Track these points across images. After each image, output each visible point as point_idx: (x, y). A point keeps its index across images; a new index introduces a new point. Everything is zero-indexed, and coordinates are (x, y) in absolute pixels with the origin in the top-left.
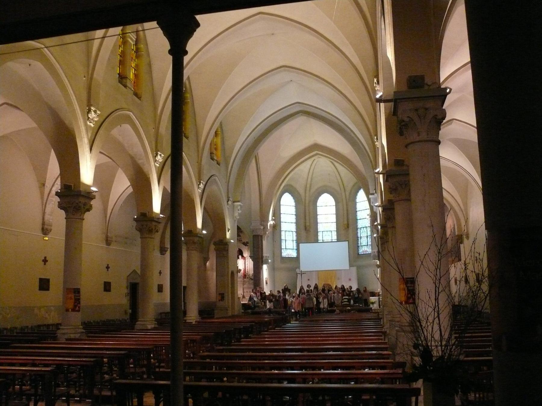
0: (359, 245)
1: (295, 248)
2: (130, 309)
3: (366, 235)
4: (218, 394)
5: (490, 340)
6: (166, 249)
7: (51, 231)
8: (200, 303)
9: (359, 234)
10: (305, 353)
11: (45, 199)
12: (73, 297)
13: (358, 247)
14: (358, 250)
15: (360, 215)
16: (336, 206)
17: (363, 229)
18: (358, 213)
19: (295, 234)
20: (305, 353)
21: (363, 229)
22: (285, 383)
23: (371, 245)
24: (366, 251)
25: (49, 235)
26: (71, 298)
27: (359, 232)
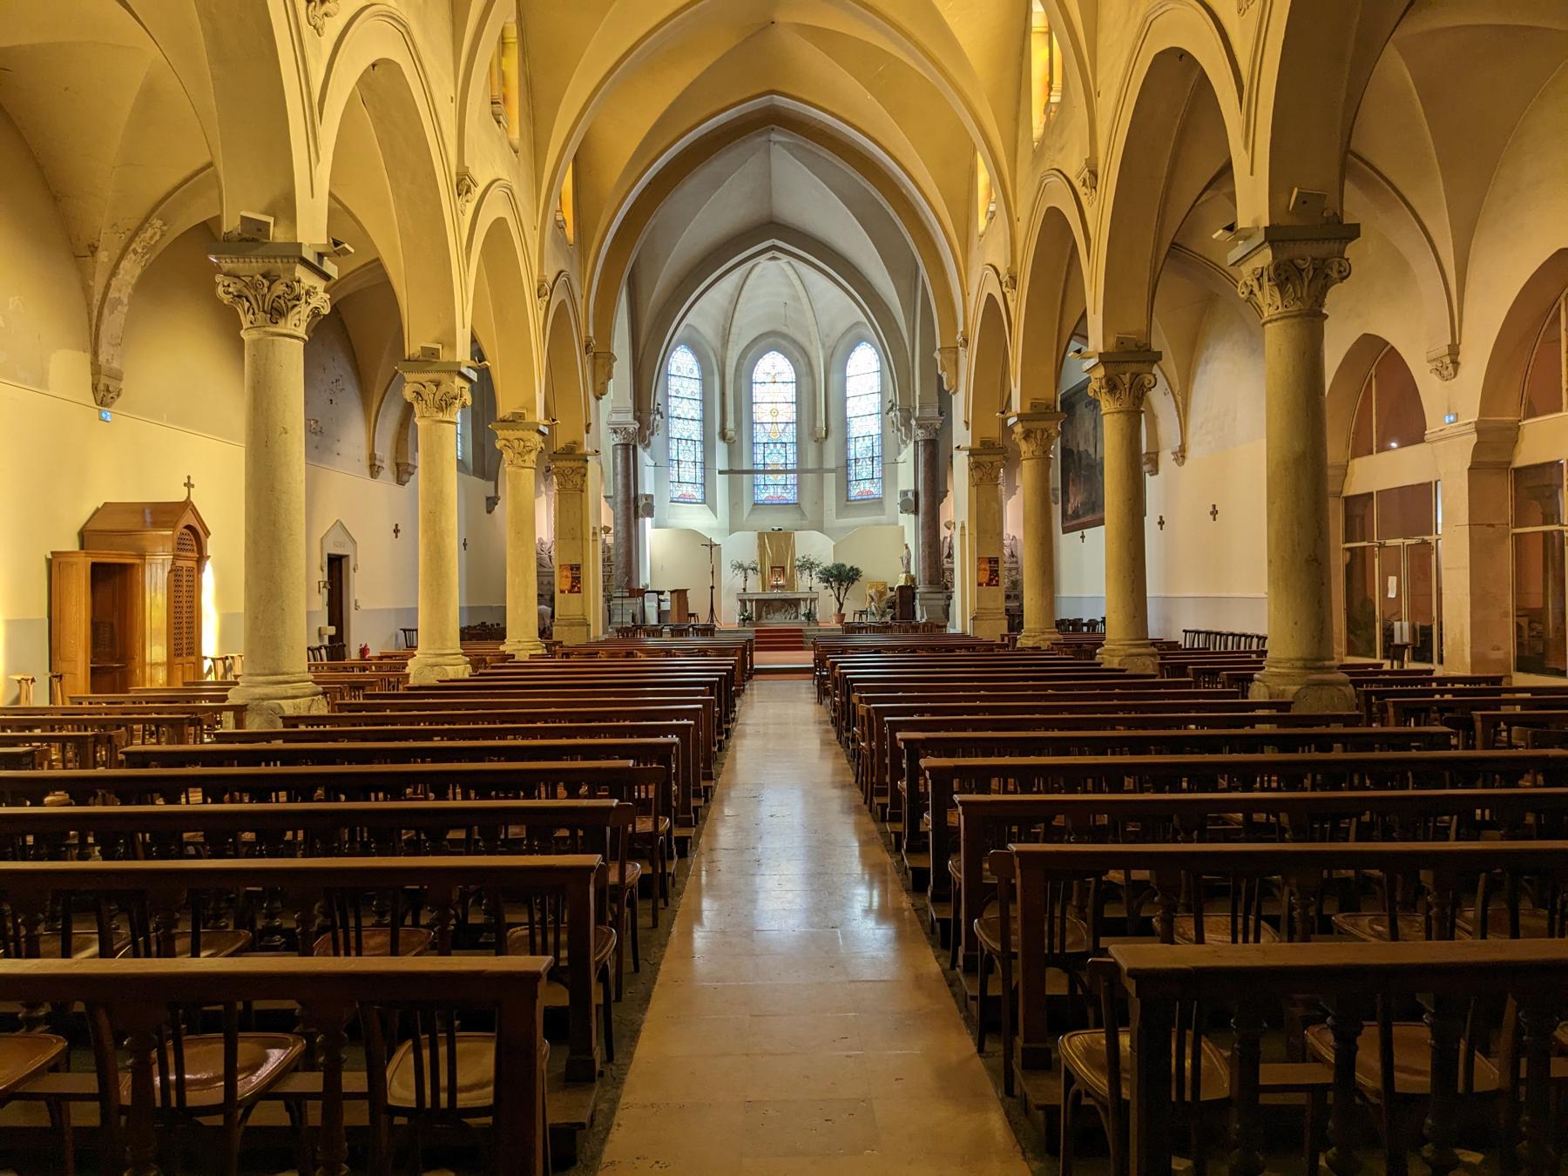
0: (852, 477)
1: (699, 480)
2: (330, 624)
3: (870, 455)
4: (285, 835)
5: (1190, 682)
6: (410, 469)
7: (118, 395)
8: (467, 611)
9: (852, 452)
10: (927, 717)
11: (97, 297)
12: (988, 568)
13: (848, 482)
14: (848, 491)
15: (853, 407)
16: (798, 382)
17: (775, 447)
18: (850, 403)
19: (699, 448)
20: (927, 717)
21: (775, 447)
22: (160, 801)
23: (881, 478)
24: (869, 493)
25: (114, 406)
26: (985, 570)
27: (852, 447)
